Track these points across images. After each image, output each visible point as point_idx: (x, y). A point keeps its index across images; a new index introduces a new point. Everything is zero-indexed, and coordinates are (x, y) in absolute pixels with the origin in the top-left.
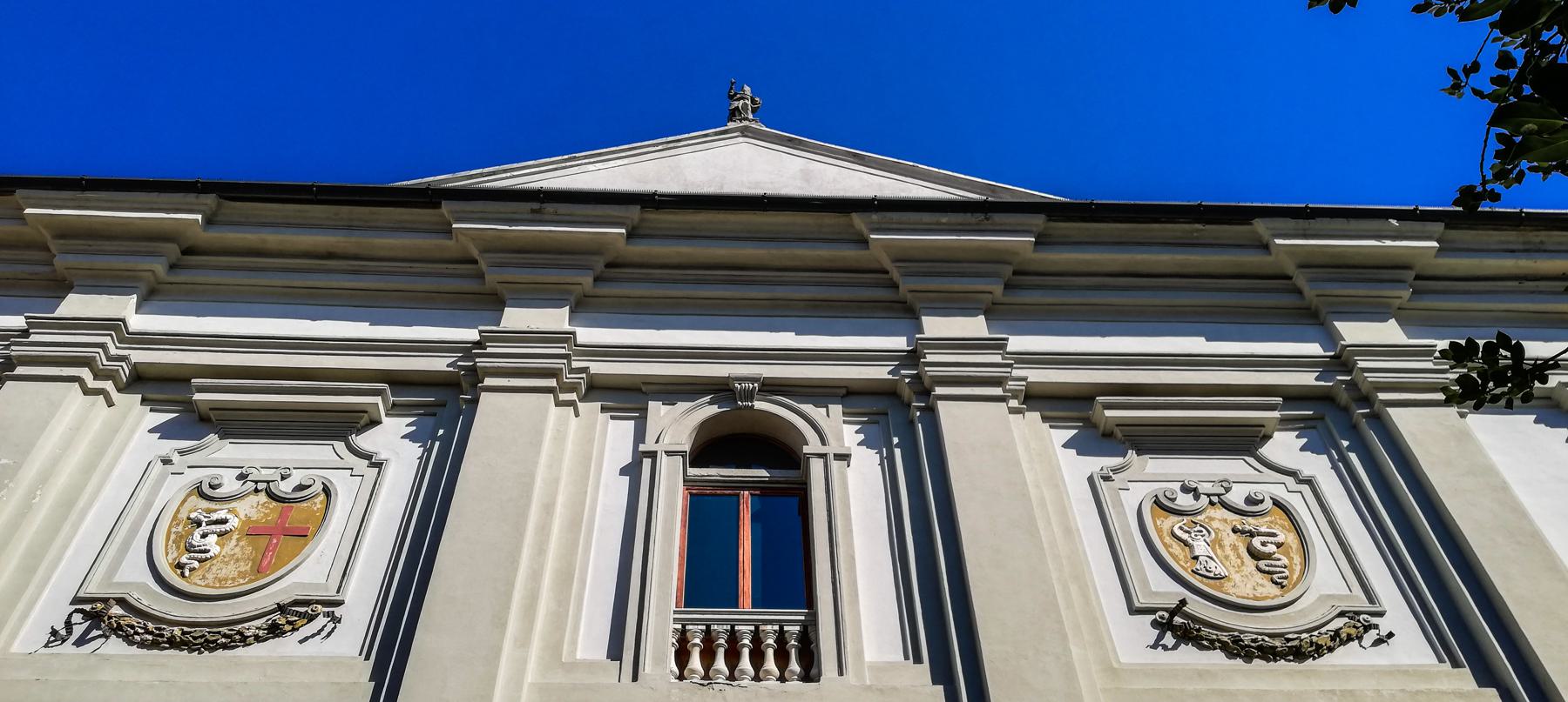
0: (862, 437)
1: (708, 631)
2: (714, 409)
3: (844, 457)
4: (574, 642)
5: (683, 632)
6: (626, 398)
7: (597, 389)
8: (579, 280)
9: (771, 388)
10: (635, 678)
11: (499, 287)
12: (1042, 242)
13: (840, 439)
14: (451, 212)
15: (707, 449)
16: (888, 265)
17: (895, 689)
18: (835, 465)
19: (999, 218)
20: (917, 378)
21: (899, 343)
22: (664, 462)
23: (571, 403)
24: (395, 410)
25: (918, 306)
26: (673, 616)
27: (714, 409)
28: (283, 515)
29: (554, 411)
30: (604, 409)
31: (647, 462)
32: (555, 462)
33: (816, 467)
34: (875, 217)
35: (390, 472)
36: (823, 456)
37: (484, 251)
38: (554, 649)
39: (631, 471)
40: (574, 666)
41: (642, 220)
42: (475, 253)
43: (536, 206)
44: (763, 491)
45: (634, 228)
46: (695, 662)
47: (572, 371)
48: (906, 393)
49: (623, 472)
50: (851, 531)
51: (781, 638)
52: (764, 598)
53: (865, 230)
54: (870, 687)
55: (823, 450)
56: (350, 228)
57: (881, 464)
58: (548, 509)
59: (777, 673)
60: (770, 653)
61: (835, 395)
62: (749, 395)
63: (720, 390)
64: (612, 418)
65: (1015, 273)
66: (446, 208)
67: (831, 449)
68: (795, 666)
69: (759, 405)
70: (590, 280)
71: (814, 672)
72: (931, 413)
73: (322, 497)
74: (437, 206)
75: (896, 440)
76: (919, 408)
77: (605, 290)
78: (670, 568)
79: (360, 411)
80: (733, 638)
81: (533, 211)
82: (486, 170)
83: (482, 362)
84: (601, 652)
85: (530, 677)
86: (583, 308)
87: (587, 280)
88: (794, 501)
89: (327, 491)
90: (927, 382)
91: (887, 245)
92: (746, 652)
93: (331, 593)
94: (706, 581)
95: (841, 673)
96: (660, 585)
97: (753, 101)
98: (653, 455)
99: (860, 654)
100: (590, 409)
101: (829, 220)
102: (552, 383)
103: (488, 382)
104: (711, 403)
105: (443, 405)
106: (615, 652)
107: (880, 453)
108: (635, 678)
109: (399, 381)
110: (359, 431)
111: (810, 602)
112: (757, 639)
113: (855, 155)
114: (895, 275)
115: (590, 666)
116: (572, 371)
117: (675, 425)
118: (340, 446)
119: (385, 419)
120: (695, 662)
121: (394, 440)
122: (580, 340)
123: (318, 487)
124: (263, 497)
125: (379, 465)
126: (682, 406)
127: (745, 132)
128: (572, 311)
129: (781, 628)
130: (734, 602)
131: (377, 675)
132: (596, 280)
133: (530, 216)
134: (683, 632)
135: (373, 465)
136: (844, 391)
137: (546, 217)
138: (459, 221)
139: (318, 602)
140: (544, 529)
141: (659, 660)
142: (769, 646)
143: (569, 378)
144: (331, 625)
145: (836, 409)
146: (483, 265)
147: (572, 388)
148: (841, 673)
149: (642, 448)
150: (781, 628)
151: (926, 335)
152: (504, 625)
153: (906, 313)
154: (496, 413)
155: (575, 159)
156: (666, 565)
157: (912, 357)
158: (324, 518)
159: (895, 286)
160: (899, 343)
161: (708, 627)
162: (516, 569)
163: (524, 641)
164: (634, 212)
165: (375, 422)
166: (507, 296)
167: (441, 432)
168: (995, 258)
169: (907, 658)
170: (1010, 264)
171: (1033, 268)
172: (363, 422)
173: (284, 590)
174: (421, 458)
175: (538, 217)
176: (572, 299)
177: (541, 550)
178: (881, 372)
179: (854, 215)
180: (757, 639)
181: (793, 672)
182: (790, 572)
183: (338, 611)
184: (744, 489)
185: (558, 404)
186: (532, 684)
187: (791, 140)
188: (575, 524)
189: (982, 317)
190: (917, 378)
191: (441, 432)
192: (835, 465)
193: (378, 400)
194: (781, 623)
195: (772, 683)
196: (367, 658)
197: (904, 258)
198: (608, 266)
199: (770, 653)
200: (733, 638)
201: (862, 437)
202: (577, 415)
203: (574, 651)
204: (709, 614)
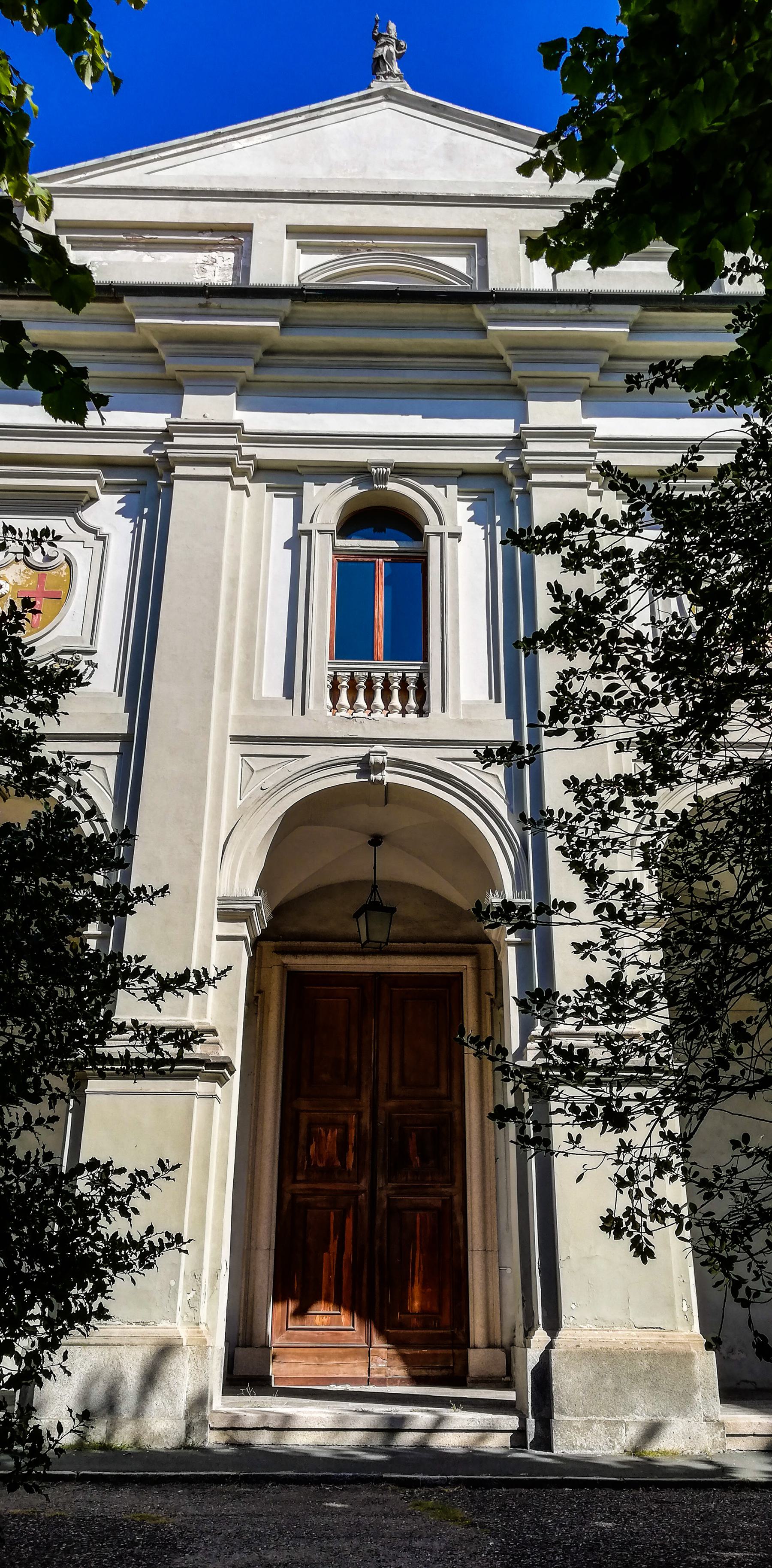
0: (472, 513)
1: (352, 676)
2: (355, 491)
3: (456, 535)
4: (260, 685)
5: (335, 677)
6: (286, 478)
7: (263, 471)
8: (243, 368)
9: (402, 471)
10: (303, 713)
11: (178, 375)
12: (636, 329)
13: (454, 517)
14: (132, 307)
15: (354, 522)
16: (502, 351)
17: (480, 722)
18: (449, 541)
19: (601, 309)
20: (519, 464)
21: (505, 427)
22: (317, 538)
23: (244, 488)
24: (108, 488)
25: (526, 390)
26: (328, 666)
27: (355, 491)
28: (41, 581)
29: (231, 494)
30: (269, 489)
31: (304, 539)
32: (236, 545)
33: (434, 544)
34: (493, 308)
35: (112, 544)
36: (440, 534)
37: (165, 341)
38: (246, 689)
39: (293, 545)
40: (261, 703)
41: (293, 312)
42: (156, 344)
43: (202, 300)
44: (394, 559)
45: (286, 318)
46: (344, 699)
47: (243, 458)
48: (510, 476)
49: (287, 546)
50: (458, 600)
51: (404, 683)
52: (394, 652)
53: (485, 322)
54: (462, 721)
55: (440, 529)
56: (49, 320)
57: (485, 539)
58: (234, 582)
59: (400, 707)
60: (396, 692)
61: (452, 476)
62: (383, 479)
63: (361, 473)
64: (276, 496)
65: (611, 358)
66: (128, 302)
67: (446, 529)
68: (412, 703)
69: (392, 486)
70: (252, 368)
71: (425, 707)
72: (527, 494)
73: (66, 566)
74: (119, 300)
75: (498, 518)
76: (518, 492)
77: (266, 375)
78: (324, 630)
79: (82, 492)
80: (370, 682)
81: (201, 306)
82: (135, 152)
83: (172, 453)
84: (278, 692)
85: (232, 711)
86: (249, 393)
87: (249, 369)
88: (419, 566)
89: (68, 560)
90: (526, 469)
91: (502, 335)
92: (379, 691)
93: (86, 645)
94: (350, 640)
95: (443, 711)
96: (318, 643)
97: (398, 47)
98: (309, 533)
99: (457, 696)
100: (258, 488)
101: (454, 310)
102: (227, 471)
103: (179, 470)
104: (352, 485)
105: (147, 484)
106: (288, 692)
107: (485, 528)
108: (303, 713)
109: (107, 464)
110: (83, 508)
111: (425, 657)
112: (387, 683)
113: (500, 125)
114: (508, 360)
115: (272, 702)
116: (243, 458)
117: (327, 502)
118: (71, 520)
119: (101, 496)
120: (344, 699)
121: (107, 511)
122: (247, 428)
123: (61, 559)
124: (22, 566)
125: (103, 538)
126: (331, 487)
127: (389, 95)
128: (238, 395)
129: (404, 675)
130: (370, 655)
131: (130, 707)
132: (257, 366)
133: (199, 311)
134: (335, 677)
135: (98, 538)
136: (460, 473)
137: (213, 311)
138: (141, 315)
139: (79, 652)
140: (232, 599)
141: (319, 700)
142: (395, 687)
143: (241, 464)
144: (90, 669)
145: (453, 489)
146: (162, 353)
147: (243, 473)
148: (443, 711)
149: (300, 527)
150: (404, 675)
151: (531, 424)
152: (211, 677)
153: (512, 395)
154: (188, 497)
155: (219, 135)
156: (321, 626)
157: (517, 443)
158: (70, 584)
159: (508, 371)
160: (505, 427)
161: (352, 673)
162: (216, 635)
163: (226, 687)
164: (286, 305)
165: (94, 500)
166: (184, 383)
167: (146, 510)
168: (594, 346)
169: (490, 698)
170: (607, 351)
171: (627, 353)
172: (85, 500)
173: (53, 642)
174: (133, 532)
175: (204, 310)
176: (238, 385)
177: (231, 618)
178: (488, 457)
179: (475, 306)
180: (387, 683)
181: (411, 707)
182: (411, 633)
183: (94, 658)
184: (378, 557)
185: (234, 488)
186: (235, 717)
187: (435, 105)
188: (253, 593)
189: (578, 402)
190: (519, 464)
191: (146, 510)
192: (449, 541)
193: (94, 483)
194: (404, 672)
195: (396, 716)
196: (120, 695)
197: (517, 346)
198: (267, 353)
199: (396, 692)
200: (370, 682)
201: (472, 513)
202: (248, 495)
203: (260, 691)
204: (354, 664)
